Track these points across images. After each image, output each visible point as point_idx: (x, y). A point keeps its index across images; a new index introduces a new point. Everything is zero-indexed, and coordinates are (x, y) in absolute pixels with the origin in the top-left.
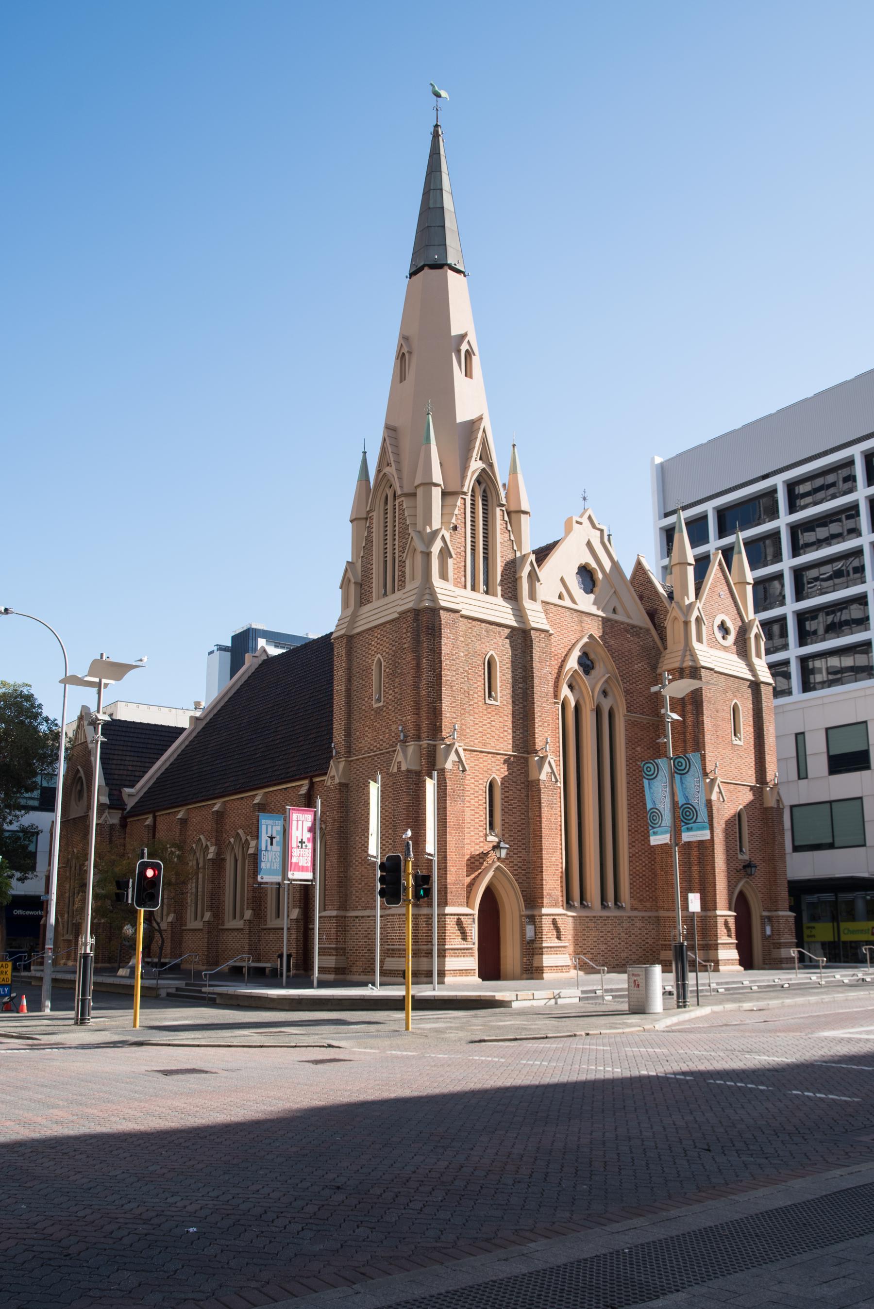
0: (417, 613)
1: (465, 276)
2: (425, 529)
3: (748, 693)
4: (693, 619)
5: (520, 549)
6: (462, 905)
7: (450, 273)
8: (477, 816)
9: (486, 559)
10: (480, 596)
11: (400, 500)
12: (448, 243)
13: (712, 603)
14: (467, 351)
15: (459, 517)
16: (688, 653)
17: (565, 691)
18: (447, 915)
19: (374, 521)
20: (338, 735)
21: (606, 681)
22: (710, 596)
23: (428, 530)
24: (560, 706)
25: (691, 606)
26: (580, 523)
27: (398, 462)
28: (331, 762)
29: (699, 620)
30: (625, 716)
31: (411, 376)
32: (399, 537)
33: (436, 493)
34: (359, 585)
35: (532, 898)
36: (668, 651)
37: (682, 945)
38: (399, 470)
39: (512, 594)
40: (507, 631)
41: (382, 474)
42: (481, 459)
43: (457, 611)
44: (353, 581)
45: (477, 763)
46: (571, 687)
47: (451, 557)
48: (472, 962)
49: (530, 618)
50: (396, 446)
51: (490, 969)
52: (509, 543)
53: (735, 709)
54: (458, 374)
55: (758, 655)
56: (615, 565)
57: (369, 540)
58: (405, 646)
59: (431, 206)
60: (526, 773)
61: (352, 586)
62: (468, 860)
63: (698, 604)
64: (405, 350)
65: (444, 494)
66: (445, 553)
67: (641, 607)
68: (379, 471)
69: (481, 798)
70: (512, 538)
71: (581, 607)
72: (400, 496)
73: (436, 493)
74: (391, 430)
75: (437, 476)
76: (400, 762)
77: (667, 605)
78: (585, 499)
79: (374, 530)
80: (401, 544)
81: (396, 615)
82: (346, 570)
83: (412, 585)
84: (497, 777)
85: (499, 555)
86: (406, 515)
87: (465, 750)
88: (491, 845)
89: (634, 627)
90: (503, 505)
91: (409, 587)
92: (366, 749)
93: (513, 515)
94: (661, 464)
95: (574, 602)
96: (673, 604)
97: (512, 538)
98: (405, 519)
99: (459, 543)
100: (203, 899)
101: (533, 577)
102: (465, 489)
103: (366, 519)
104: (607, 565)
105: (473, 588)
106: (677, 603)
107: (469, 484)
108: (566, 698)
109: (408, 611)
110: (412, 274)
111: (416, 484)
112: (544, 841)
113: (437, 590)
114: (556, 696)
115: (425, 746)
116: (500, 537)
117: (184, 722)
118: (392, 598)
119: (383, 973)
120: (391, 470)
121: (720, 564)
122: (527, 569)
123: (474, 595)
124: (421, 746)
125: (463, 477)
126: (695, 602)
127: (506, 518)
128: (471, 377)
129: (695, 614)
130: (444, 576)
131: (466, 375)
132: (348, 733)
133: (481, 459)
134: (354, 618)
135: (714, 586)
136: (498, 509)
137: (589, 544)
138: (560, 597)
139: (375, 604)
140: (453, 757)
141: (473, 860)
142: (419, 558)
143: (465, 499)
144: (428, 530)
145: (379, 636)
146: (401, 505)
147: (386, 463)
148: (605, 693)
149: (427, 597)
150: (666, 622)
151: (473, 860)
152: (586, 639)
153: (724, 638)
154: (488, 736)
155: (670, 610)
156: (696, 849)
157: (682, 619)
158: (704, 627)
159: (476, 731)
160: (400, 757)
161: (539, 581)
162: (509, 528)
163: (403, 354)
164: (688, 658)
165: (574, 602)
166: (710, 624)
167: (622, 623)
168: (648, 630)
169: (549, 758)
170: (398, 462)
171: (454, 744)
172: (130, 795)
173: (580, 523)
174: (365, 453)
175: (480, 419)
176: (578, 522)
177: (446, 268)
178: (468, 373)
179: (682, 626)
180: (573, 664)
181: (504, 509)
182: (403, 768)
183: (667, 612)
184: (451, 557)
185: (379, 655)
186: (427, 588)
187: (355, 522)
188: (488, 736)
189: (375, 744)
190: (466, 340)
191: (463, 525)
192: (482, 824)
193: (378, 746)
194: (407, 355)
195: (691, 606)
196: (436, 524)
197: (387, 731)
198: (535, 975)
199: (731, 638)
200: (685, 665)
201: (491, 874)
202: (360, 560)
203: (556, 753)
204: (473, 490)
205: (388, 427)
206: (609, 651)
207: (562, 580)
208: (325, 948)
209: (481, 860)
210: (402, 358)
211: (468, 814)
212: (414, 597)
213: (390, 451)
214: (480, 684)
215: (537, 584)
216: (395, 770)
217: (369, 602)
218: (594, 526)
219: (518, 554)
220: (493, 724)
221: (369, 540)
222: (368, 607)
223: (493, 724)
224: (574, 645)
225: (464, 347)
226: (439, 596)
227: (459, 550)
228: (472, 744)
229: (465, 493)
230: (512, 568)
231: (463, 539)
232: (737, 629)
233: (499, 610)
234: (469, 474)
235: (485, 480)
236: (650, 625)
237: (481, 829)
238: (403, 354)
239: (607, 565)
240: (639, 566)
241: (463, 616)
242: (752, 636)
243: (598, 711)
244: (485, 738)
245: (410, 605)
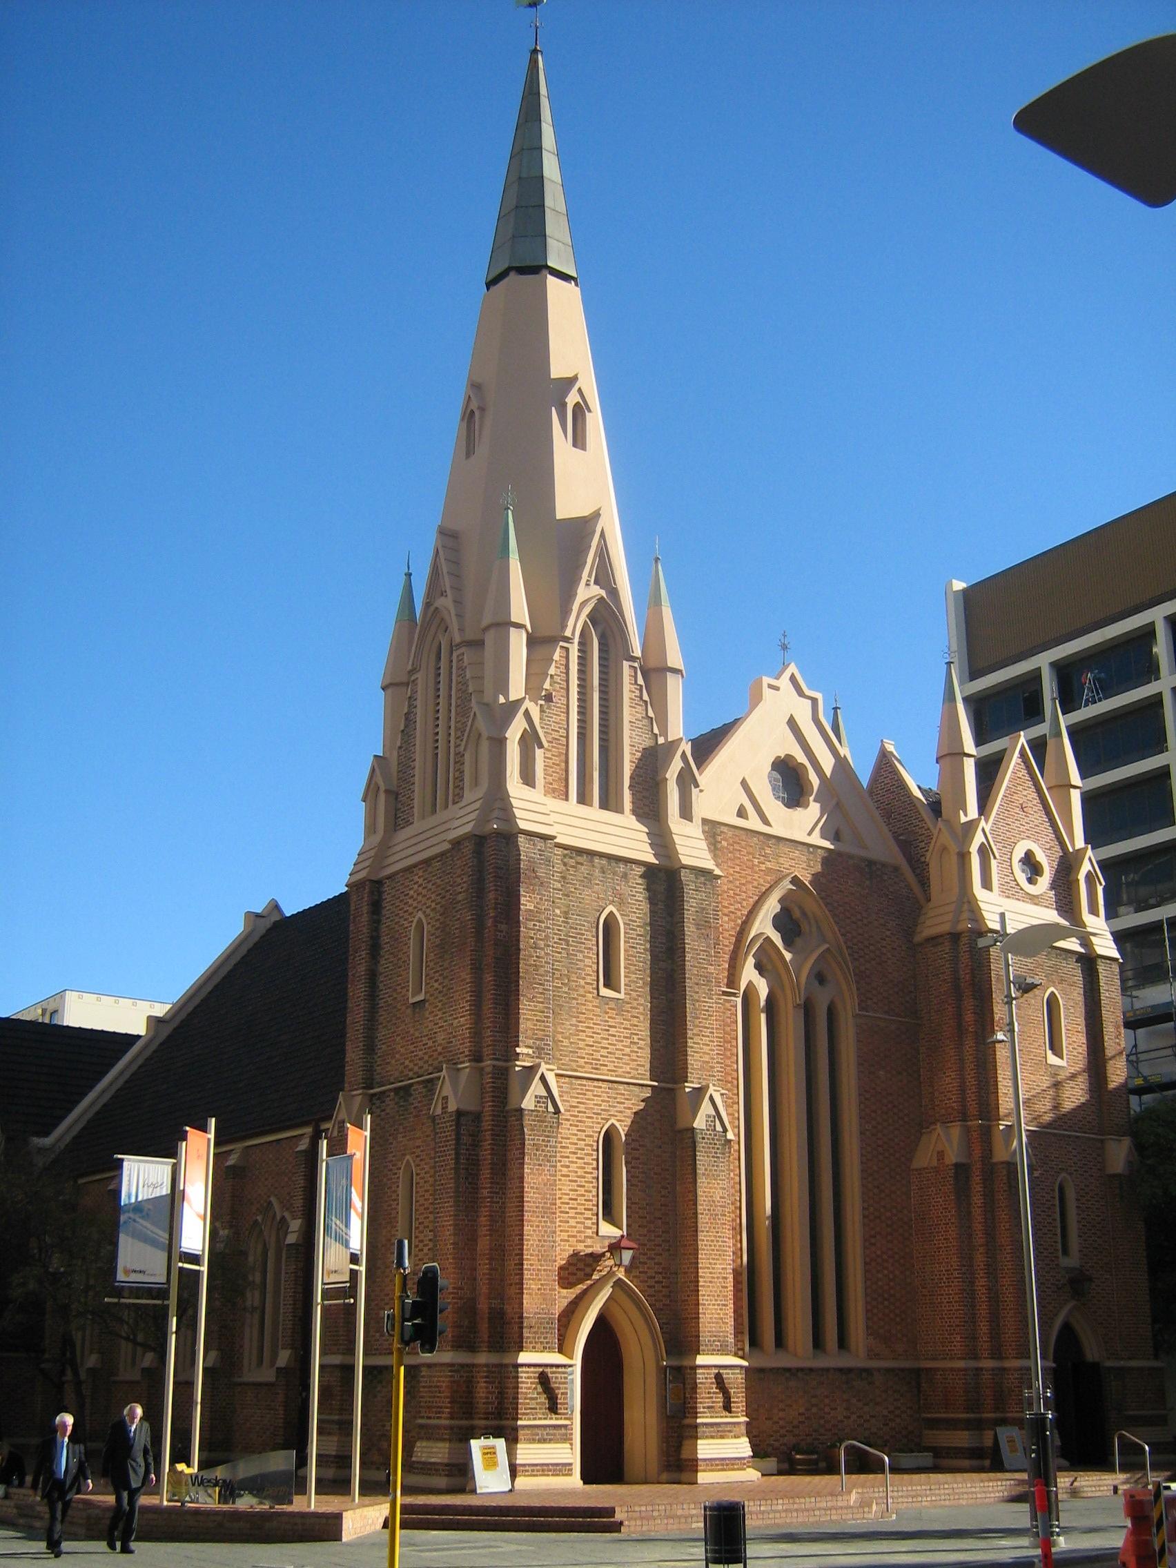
0: (479, 841)
1: (577, 285)
2: (497, 699)
3: (1075, 973)
4: (974, 849)
5: (664, 732)
6: (551, 1350)
7: (551, 280)
8: (582, 1191)
9: (604, 749)
10: (594, 812)
11: (459, 652)
12: (548, 231)
13: (1009, 821)
14: (577, 405)
15: (557, 679)
16: (965, 907)
17: (749, 974)
18: (522, 1365)
19: (419, 687)
20: (353, 1055)
21: (822, 956)
22: (1004, 809)
23: (502, 700)
24: (739, 1000)
25: (971, 826)
26: (777, 689)
28: (341, 1099)
29: (984, 851)
30: (855, 1016)
31: (482, 449)
32: (457, 714)
34: (394, 795)
35: (680, 1337)
36: (931, 905)
37: (1043, 1418)
38: (457, 602)
39: (650, 809)
40: (642, 869)
41: (432, 609)
42: (596, 583)
43: (545, 838)
44: (382, 788)
45: (581, 1099)
46: (759, 967)
47: (541, 746)
48: (570, 1453)
49: (680, 849)
50: (456, 562)
51: (603, 1461)
52: (645, 722)
55: (1094, 911)
56: (841, 762)
57: (409, 718)
58: (460, 897)
59: (524, 175)
60: (673, 1120)
61: (382, 797)
62: (561, 1268)
63: (983, 823)
64: (474, 405)
65: (532, 642)
66: (530, 740)
67: (885, 829)
68: (427, 605)
69: (588, 1159)
70: (651, 714)
71: (776, 830)
72: (459, 645)
74: (450, 538)
75: (520, 610)
76: (446, 1098)
77: (931, 826)
78: (784, 647)
79: (418, 703)
80: (459, 725)
81: (447, 846)
82: (373, 770)
83: (473, 796)
84: (617, 1124)
85: (626, 742)
86: (468, 676)
87: (557, 1075)
88: (607, 1243)
89: (871, 863)
90: (633, 659)
91: (469, 796)
92: (397, 1074)
93: (653, 676)
94: (965, 591)
95: (766, 822)
96: (940, 824)
97: (651, 714)
98: (466, 684)
99: (562, 723)
101: (687, 781)
102: (568, 633)
103: (408, 684)
104: (827, 763)
105: (583, 799)
106: (947, 822)
107: (575, 623)
108: (750, 984)
109: (467, 837)
110: (489, 285)
111: (485, 622)
112: (701, 1236)
113: (514, 802)
114: (732, 981)
115: (489, 1069)
116: (630, 713)
117: (138, 1027)
118: (442, 815)
119: (408, 1467)
120: (445, 603)
121: (1023, 754)
122: (676, 765)
123: (583, 810)
124: (482, 1069)
125: (565, 612)
126: (978, 820)
127: (641, 681)
128: (584, 448)
129: (979, 839)
130: (528, 778)
131: (575, 445)
132: (370, 1049)
133: (596, 583)
134: (375, 854)
135: (1010, 793)
136: (626, 664)
137: (792, 723)
138: (741, 813)
139: (417, 826)
140: (536, 1088)
141: (572, 1269)
142: (485, 746)
143: (567, 650)
144: (502, 700)
145: (421, 881)
146: (460, 660)
148: (820, 978)
149: (496, 813)
150: (928, 854)
151: (572, 1269)
152: (787, 885)
153: (1031, 881)
154: (604, 1052)
155: (935, 832)
156: (981, 1250)
157: (954, 848)
158: (994, 863)
159: (581, 1044)
160: (447, 1090)
161: (697, 786)
162: (646, 697)
164: (965, 915)
165: (766, 822)
166: (1006, 858)
167: (851, 857)
168: (896, 869)
169: (711, 1090)
170: (458, 589)
171: (539, 1066)
172: (41, 1150)
173: (777, 689)
174: (409, 575)
175: (596, 515)
176: (770, 686)
177: (545, 272)
178: (579, 441)
179: (954, 859)
180: (764, 925)
181: (636, 665)
182: (452, 1107)
183: (930, 837)
184: (541, 746)
185: (420, 914)
186: (498, 801)
187: (389, 691)
188: (604, 1052)
189: (411, 1065)
190: (575, 390)
191: (563, 692)
192: (589, 1205)
193: (416, 1069)
194: (477, 414)
195: (971, 826)
196: (517, 688)
197: (430, 1043)
198: (685, 1476)
199: (1045, 881)
200: (960, 927)
201: (606, 1292)
202: (395, 754)
203: (727, 1081)
204: (582, 634)
205: (442, 532)
206: (827, 905)
207: (744, 783)
208: (328, 1422)
209: (588, 1270)
210: (469, 417)
211: (565, 1187)
212: (473, 816)
213: (445, 571)
214: (590, 960)
215: (695, 791)
216: (439, 1111)
217: (409, 823)
218: (801, 693)
219: (661, 740)
220: (612, 1031)
221: (409, 718)
222: (408, 831)
223: (612, 1031)
224: (763, 897)
225: (572, 399)
226: (517, 813)
227: (555, 735)
228: (574, 1065)
229: (567, 640)
230: (652, 763)
231: (563, 716)
232: (1055, 864)
233: (623, 835)
234: (576, 607)
235: (606, 619)
236: (898, 859)
237: (588, 1214)
238: (472, 412)
239: (827, 763)
240: (885, 764)
241: (559, 846)
242: (1082, 877)
243: (808, 1009)
244: (597, 1055)
245: (467, 829)
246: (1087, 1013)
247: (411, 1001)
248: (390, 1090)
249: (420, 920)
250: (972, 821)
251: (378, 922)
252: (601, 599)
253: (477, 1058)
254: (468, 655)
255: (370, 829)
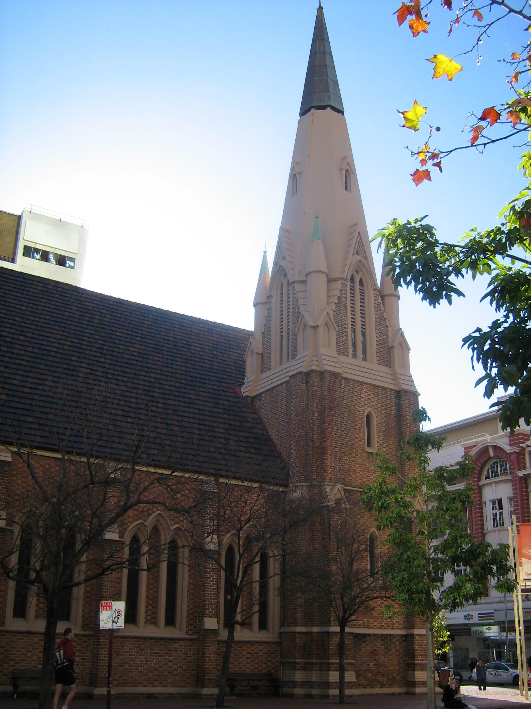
92: (357, 484)
111: (307, 272)
248: (358, 491)
254: (298, 287)
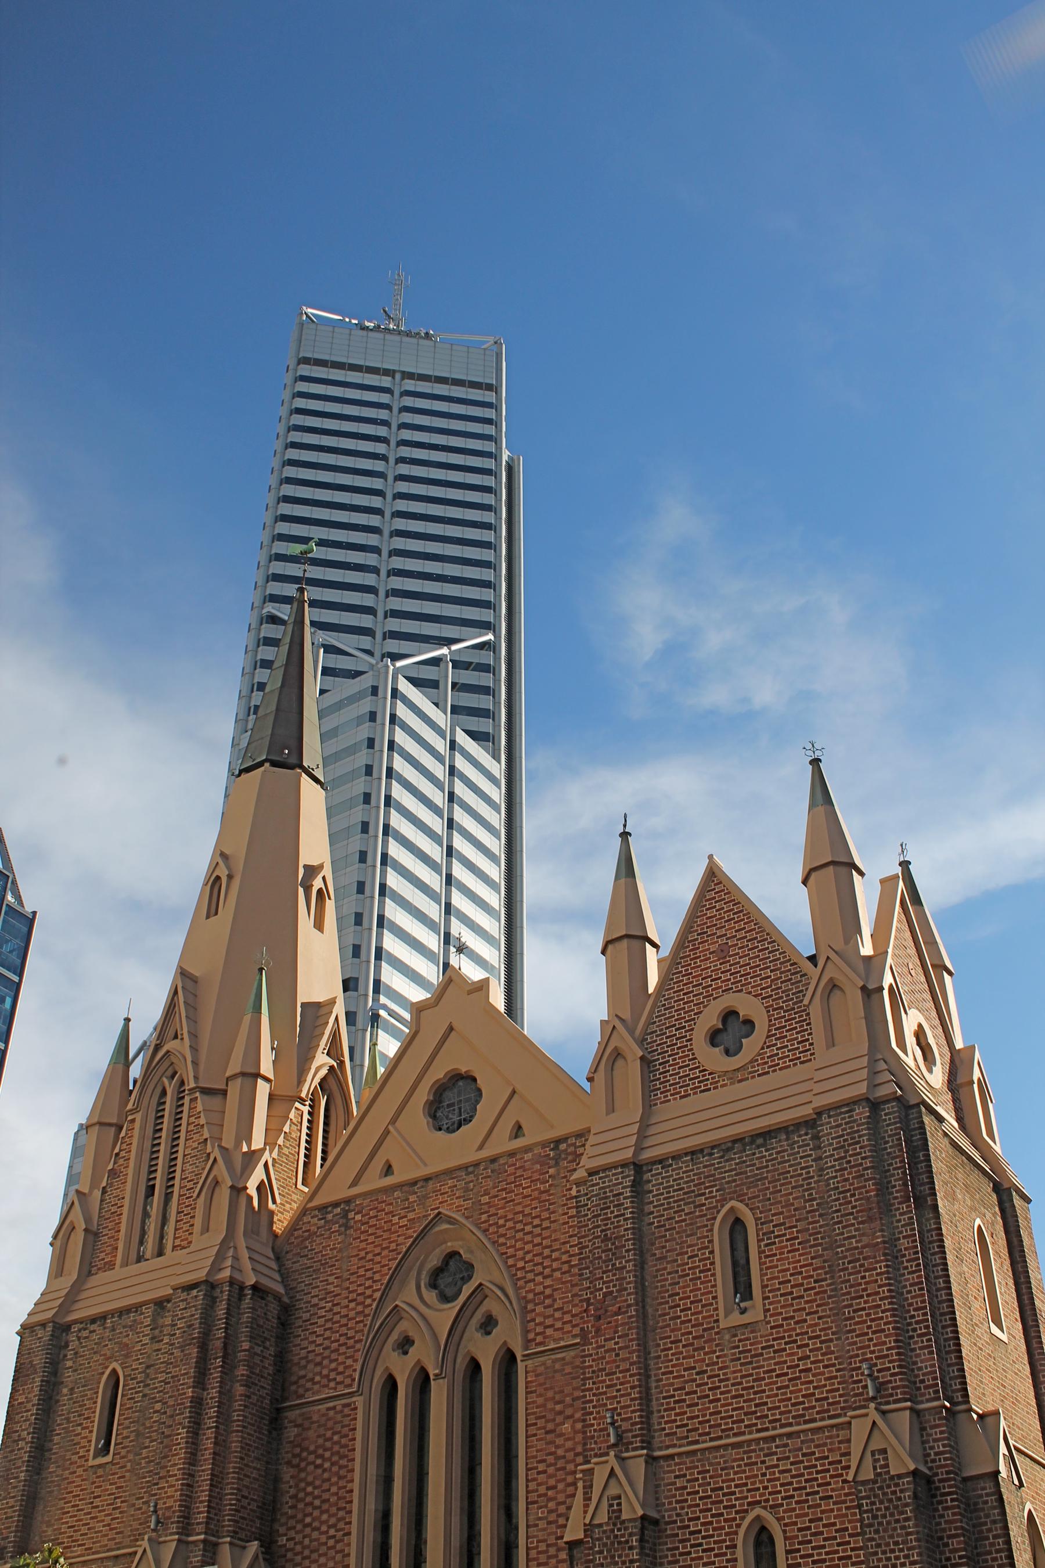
23: (245, 1149)
25: (253, 1156)
27: (194, 1036)
33: (263, 1090)
38: (194, 1049)
53: (742, 1288)
54: (305, 922)
73: (263, 1090)
91: (198, 1241)
100: (223, 1416)
111: (227, 1074)
120: (180, 1047)
147: (172, 1034)
163: (218, 878)
178: (319, 925)
195: (253, 1156)
196: (258, 1141)
205: (183, 973)
217: (110, 1266)
225: (317, 884)
238: (218, 878)
246: (76, 1199)
247: (91, 1463)
249: (114, 1371)
250: (254, 1151)
251: (417, 1515)
252: (332, 1067)
253: (186, 1527)
255: (58, 1268)
